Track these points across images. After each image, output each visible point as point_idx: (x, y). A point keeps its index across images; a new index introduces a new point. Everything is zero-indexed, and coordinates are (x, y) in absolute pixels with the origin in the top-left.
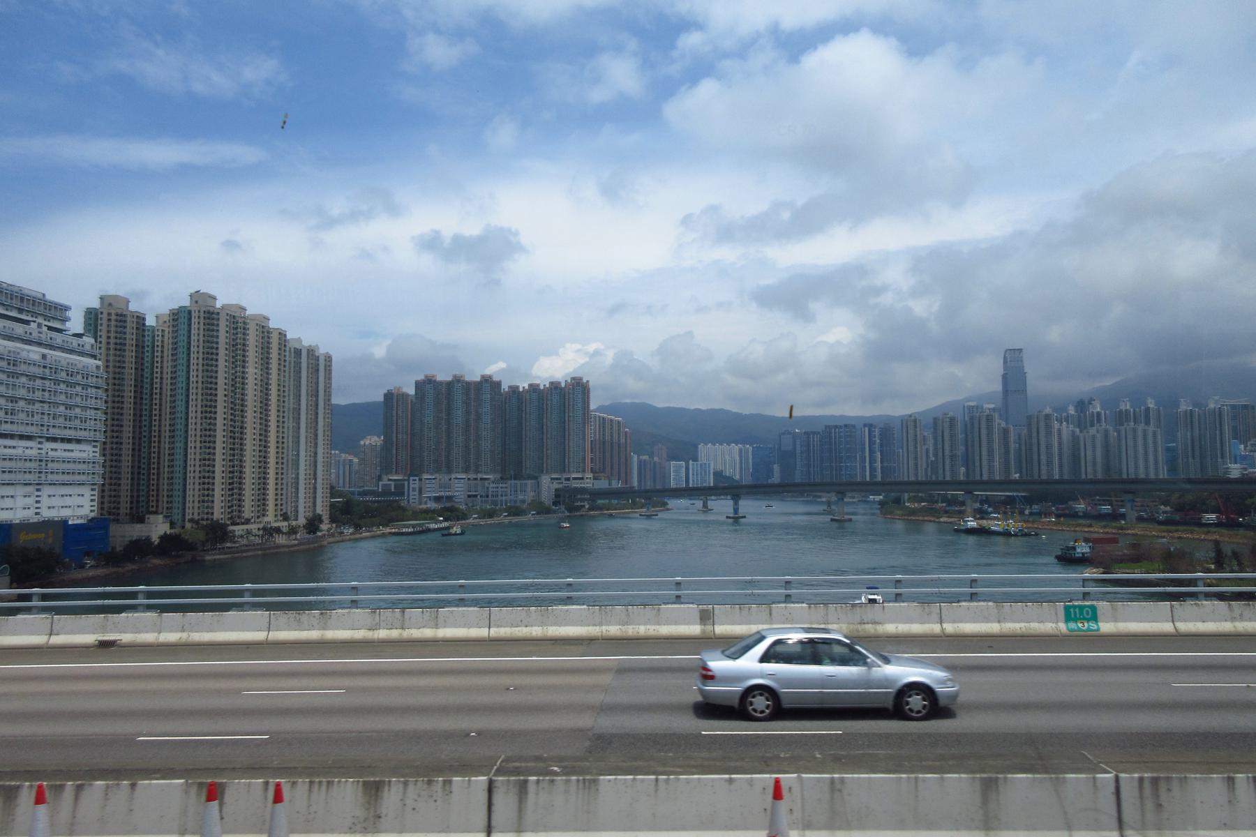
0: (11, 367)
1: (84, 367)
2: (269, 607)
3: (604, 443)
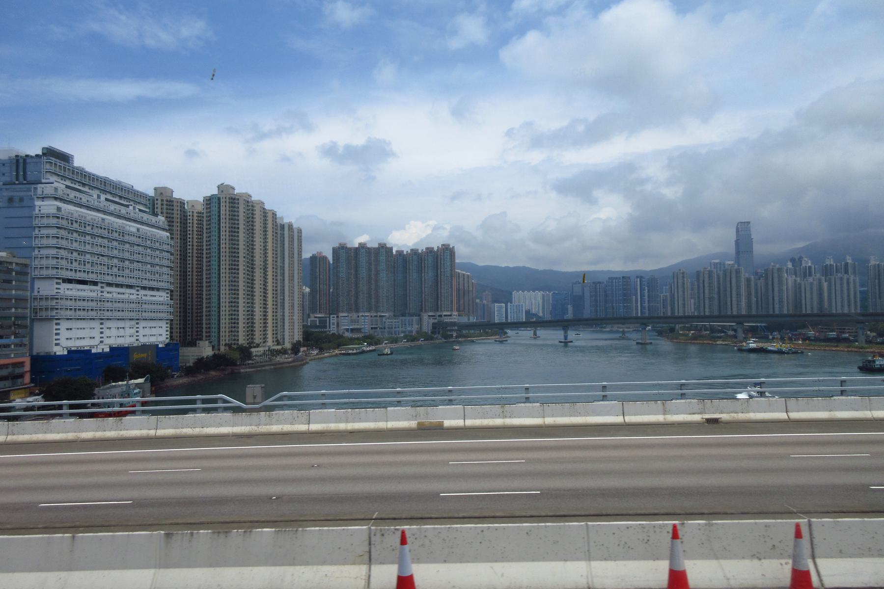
0: (121, 237)
1: (160, 237)
2: (339, 406)
3: (459, 290)
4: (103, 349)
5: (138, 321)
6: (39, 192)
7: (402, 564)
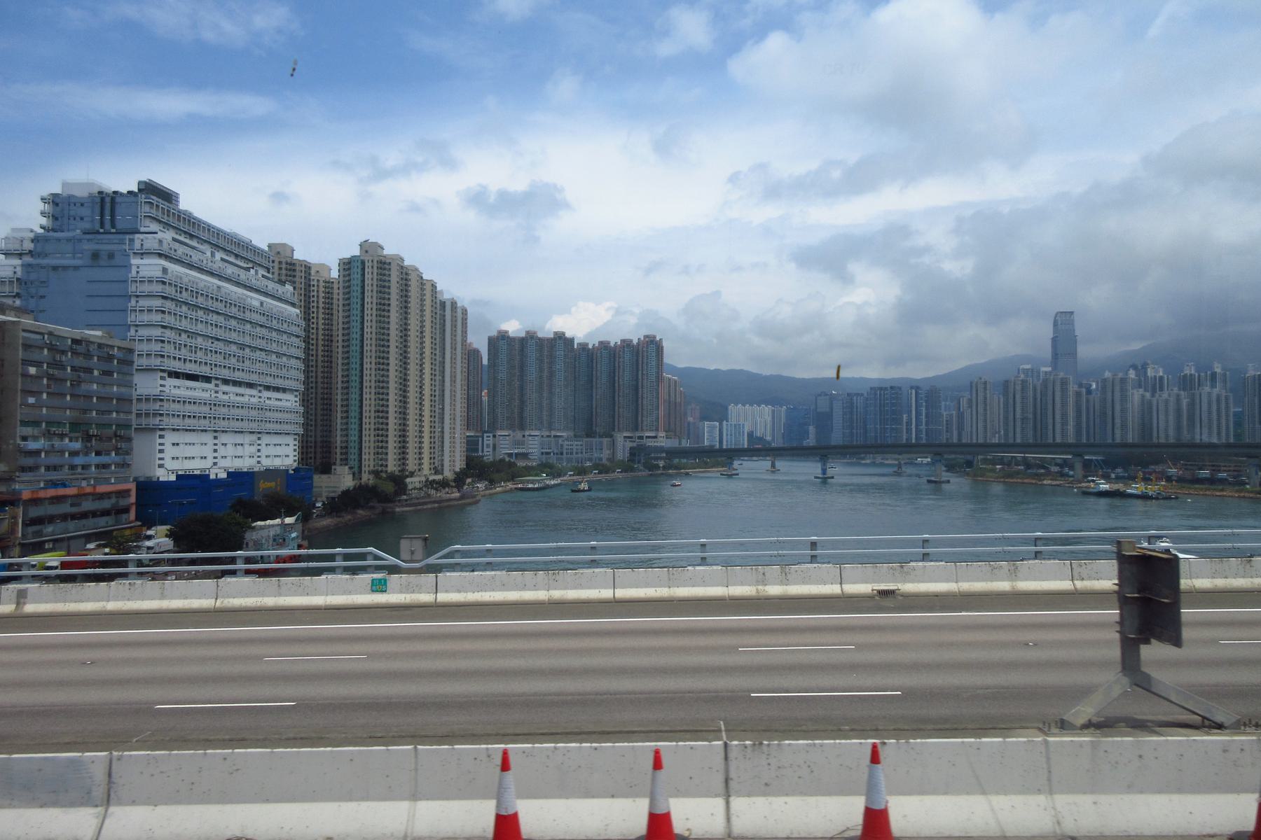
3: (670, 402)
4: (217, 474)
5: (259, 436)
6: (137, 245)
7: (871, 789)
